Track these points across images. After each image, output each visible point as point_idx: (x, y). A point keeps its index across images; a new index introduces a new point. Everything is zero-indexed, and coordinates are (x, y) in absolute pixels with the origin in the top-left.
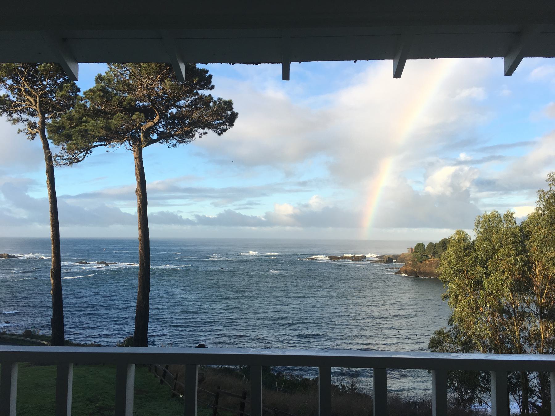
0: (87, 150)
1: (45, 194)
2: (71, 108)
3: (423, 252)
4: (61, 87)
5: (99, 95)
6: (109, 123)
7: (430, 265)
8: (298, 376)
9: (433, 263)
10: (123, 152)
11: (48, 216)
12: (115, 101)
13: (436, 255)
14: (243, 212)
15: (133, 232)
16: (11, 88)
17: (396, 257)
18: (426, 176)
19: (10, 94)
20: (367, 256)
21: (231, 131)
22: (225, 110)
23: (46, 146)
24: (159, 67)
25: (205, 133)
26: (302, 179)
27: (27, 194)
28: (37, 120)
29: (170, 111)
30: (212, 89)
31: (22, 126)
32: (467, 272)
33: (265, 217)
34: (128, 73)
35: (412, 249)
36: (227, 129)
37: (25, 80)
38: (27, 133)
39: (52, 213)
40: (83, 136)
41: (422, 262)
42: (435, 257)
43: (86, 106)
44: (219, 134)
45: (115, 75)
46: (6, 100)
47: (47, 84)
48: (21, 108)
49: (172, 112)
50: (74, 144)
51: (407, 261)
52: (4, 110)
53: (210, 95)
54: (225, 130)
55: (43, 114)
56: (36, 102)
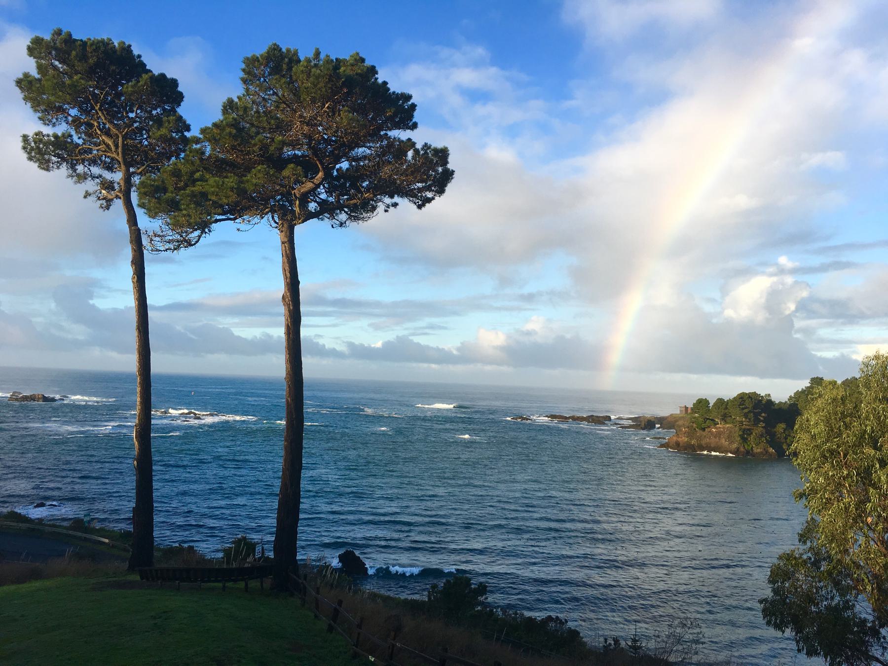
0: (204, 226)
1: (130, 301)
2: (173, 158)
3: (704, 412)
4: (159, 122)
5: (230, 133)
6: (242, 182)
7: (719, 435)
8: (505, 608)
9: (723, 433)
10: (261, 234)
11: (132, 338)
12: (255, 145)
13: (728, 419)
14: (422, 340)
15: (276, 366)
16: (76, 123)
17: (661, 420)
18: (724, 291)
19: (73, 133)
20: (613, 417)
21: (439, 205)
22: (433, 167)
23: (132, 220)
24: (331, 88)
25: (395, 205)
26: (526, 290)
27: (91, 302)
28: (118, 177)
29: (338, 166)
30: (412, 129)
31: (91, 185)
32: (845, 455)
33: (458, 349)
34: (274, 98)
35: (686, 408)
36: (433, 199)
37: (100, 109)
38: (99, 198)
39: (139, 332)
40: (198, 204)
41: (704, 429)
42: (726, 422)
43: (203, 153)
44: (420, 207)
45: (254, 102)
46: (66, 142)
47: (136, 117)
48: (90, 156)
49: (341, 168)
50: (184, 216)
51: (680, 427)
52: (63, 159)
53: (409, 140)
54: (429, 200)
55: (128, 165)
56: (117, 146)
